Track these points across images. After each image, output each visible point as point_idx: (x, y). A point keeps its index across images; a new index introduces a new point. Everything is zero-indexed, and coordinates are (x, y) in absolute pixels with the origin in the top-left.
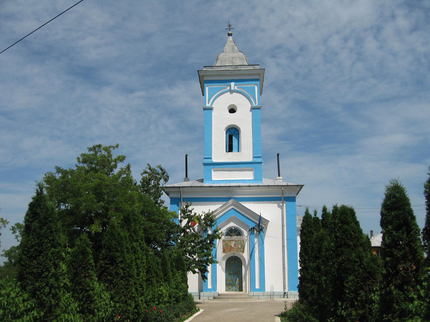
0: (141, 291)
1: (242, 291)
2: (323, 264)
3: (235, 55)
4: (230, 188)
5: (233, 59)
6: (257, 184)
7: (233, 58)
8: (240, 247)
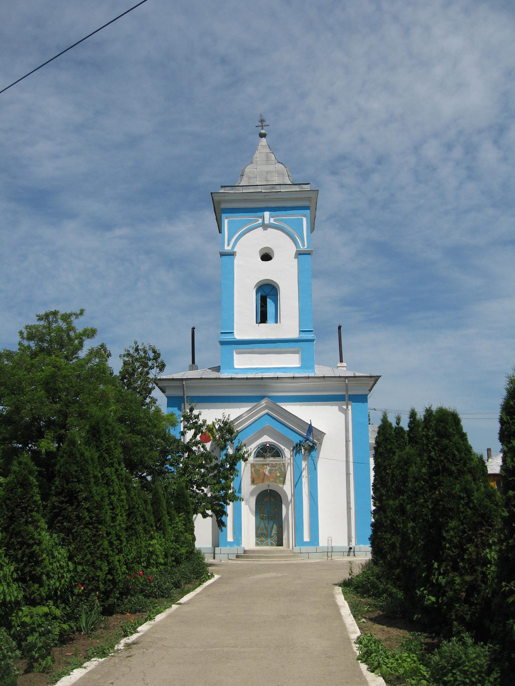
0: (118, 546)
1: (282, 545)
3: (271, 168)
4: (264, 380)
5: (267, 173)
7: (267, 172)
8: (278, 475)
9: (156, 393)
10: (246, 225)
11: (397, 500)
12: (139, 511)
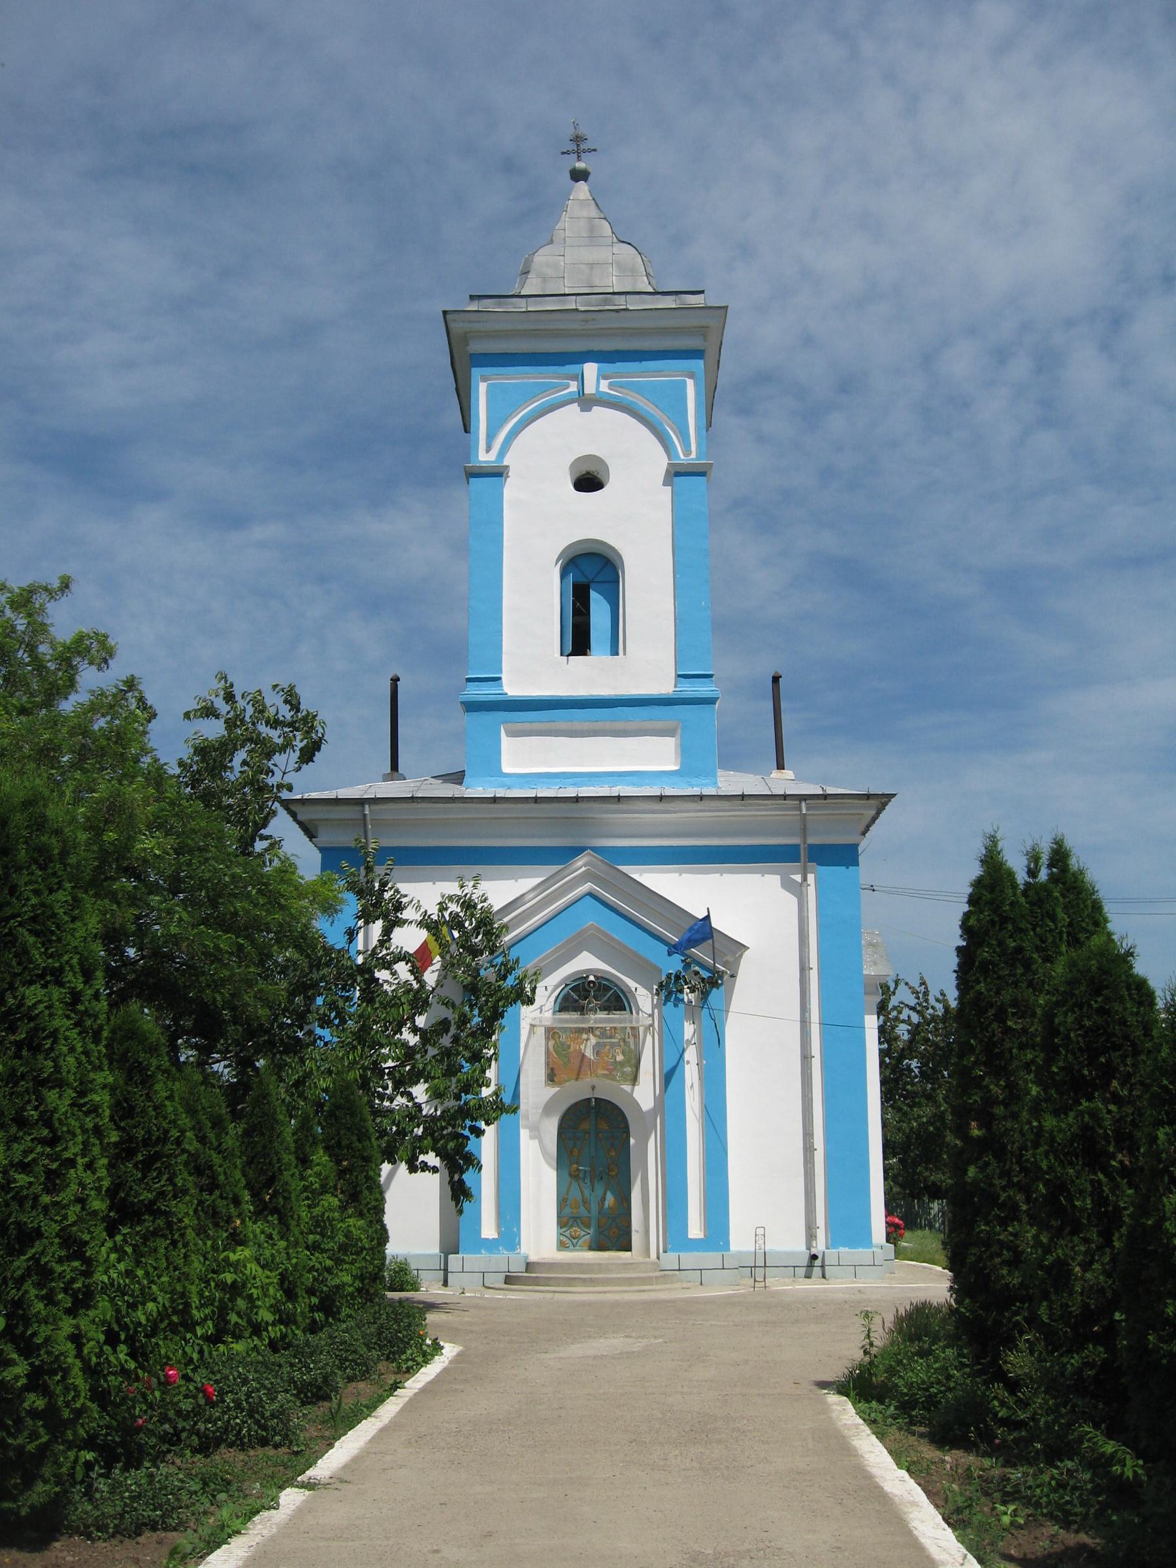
0: (73, 1280)
1: (628, 1248)
2: (1167, 1113)
3: (603, 254)
4: (581, 805)
5: (592, 269)
6: (696, 791)
7: (592, 265)
8: (620, 1058)
9: (282, 826)
10: (534, 397)
11: (1072, 1114)
12: (184, 1151)
